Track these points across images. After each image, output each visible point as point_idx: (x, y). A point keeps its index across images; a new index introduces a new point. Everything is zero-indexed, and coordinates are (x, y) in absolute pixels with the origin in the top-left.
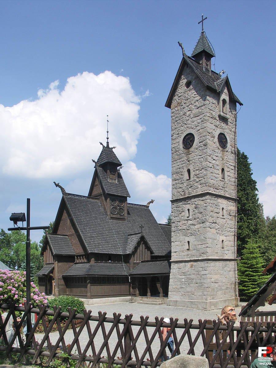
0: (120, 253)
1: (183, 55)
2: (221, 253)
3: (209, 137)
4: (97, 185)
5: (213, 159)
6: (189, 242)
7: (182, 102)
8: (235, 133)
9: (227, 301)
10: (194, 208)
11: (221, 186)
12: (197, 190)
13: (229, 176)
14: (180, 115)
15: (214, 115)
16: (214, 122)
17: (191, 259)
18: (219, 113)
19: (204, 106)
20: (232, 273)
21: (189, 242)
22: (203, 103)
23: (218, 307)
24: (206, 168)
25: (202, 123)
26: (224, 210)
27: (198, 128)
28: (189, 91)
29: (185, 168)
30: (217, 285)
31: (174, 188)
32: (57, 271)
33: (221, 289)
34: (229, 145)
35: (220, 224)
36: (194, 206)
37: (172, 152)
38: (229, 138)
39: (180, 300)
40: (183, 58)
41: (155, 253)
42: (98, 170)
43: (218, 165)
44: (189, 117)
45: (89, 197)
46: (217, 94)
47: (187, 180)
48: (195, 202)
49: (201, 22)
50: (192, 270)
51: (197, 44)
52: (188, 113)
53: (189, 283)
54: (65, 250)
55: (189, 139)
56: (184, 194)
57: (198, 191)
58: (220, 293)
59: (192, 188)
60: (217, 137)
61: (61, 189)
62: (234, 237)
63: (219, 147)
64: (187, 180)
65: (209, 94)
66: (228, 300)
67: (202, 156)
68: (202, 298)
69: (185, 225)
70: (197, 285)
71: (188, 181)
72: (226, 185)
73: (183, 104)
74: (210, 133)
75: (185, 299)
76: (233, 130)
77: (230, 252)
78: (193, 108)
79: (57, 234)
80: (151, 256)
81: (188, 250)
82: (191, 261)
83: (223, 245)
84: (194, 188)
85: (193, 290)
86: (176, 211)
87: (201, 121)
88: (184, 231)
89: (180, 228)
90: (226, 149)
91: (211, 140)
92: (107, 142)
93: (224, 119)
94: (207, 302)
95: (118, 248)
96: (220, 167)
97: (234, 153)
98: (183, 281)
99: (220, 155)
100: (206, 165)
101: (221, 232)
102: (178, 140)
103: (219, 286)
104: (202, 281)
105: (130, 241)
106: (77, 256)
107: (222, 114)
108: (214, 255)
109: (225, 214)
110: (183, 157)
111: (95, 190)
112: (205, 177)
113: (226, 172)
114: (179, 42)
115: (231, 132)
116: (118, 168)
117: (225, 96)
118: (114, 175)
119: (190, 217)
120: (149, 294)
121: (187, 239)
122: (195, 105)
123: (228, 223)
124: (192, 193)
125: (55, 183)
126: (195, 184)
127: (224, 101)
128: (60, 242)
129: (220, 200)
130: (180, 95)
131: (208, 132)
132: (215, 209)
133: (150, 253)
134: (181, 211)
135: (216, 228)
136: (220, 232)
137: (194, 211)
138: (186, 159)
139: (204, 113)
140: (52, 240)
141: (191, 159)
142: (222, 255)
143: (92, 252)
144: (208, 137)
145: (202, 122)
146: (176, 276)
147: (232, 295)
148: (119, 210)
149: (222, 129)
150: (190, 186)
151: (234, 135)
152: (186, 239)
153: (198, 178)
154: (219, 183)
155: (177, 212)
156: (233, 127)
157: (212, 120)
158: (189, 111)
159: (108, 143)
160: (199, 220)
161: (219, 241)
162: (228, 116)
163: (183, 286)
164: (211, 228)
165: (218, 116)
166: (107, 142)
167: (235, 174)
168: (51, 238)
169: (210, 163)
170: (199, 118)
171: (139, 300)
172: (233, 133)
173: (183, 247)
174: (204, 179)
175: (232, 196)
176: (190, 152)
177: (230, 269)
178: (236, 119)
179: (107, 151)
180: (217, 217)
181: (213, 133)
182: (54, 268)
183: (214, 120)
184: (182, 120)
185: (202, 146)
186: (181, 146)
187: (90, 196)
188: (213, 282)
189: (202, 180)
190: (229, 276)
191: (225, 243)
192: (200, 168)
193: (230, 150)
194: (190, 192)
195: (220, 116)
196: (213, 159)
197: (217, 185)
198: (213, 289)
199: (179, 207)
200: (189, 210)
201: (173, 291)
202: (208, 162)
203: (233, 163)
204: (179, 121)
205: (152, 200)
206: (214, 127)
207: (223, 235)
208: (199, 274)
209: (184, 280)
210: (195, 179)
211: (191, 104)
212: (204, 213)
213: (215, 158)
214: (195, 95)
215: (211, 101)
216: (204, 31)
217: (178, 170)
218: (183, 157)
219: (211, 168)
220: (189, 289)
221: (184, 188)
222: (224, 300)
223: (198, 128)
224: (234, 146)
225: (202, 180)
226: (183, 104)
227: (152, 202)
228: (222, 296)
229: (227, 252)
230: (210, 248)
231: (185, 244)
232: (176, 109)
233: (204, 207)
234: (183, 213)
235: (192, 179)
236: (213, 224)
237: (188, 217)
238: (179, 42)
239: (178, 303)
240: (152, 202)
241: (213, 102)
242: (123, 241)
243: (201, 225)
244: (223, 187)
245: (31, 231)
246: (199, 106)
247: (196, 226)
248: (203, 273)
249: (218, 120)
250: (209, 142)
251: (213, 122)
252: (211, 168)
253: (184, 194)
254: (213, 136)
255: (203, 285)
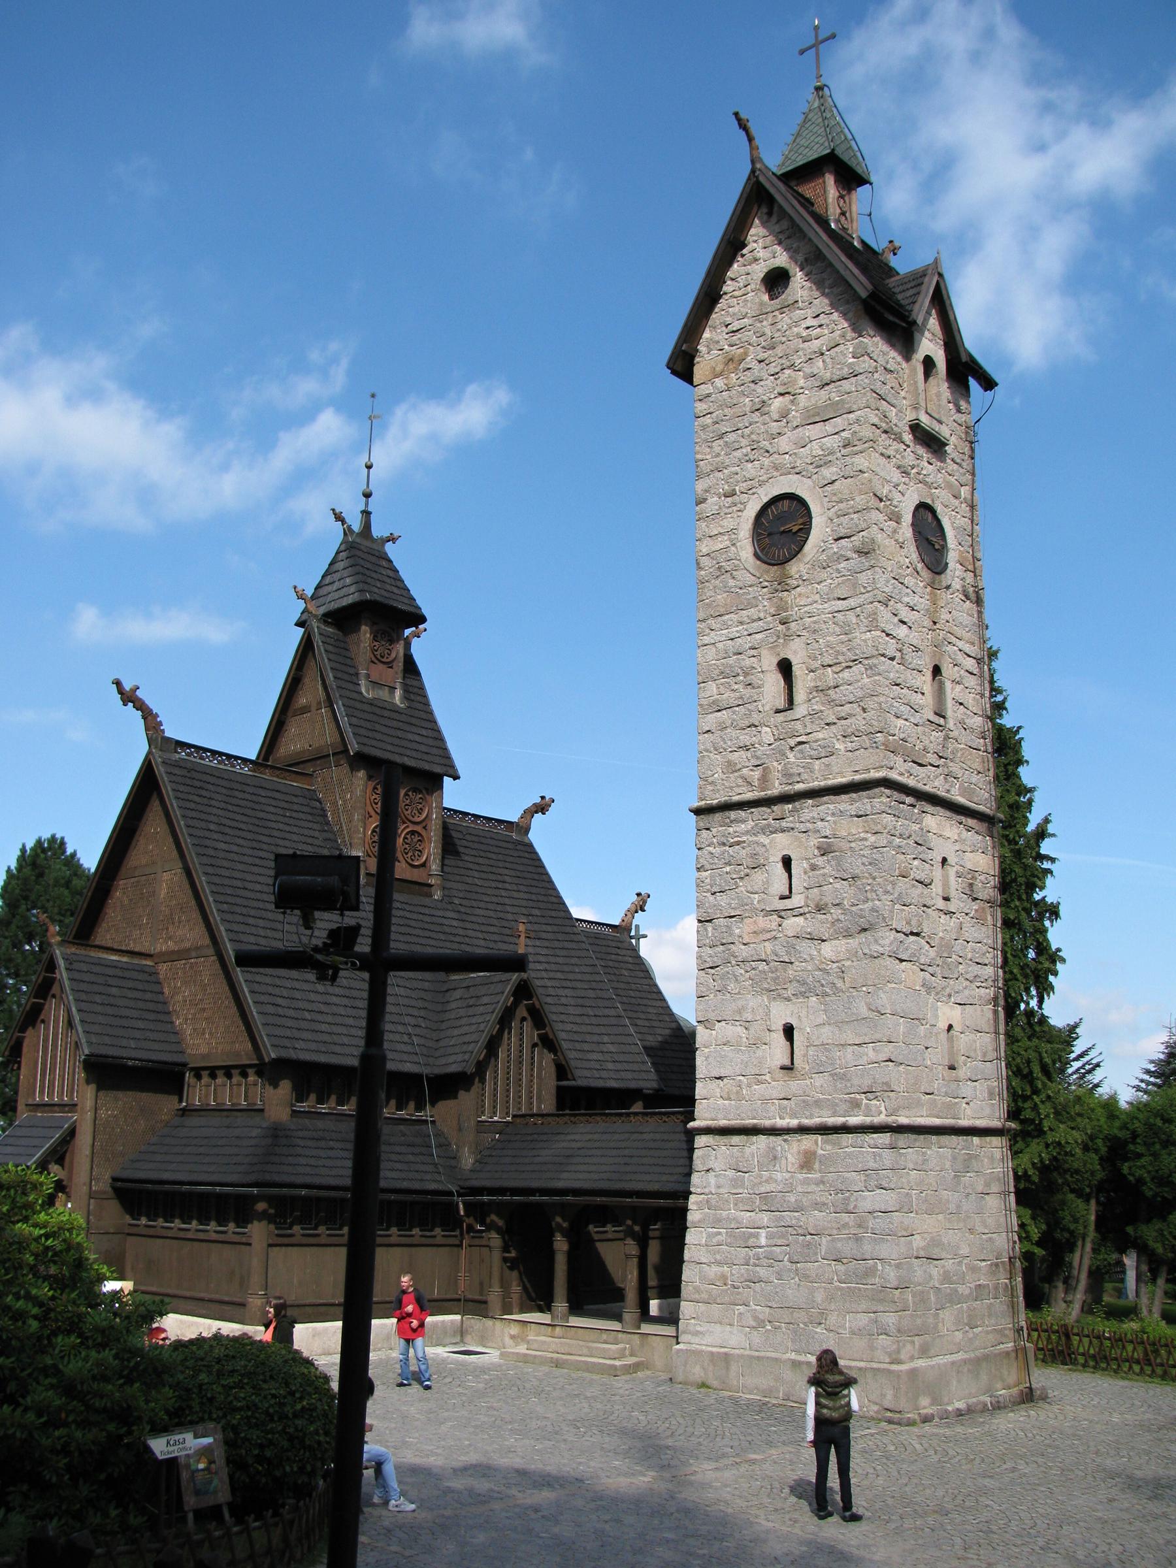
0: (414, 1069)
1: (753, 162)
2: (946, 1094)
3: (881, 517)
4: (305, 710)
5: (896, 620)
6: (789, 1031)
7: (746, 354)
8: (972, 507)
9: (984, 1364)
10: (816, 852)
11: (932, 747)
12: (828, 765)
13: (961, 704)
14: (738, 410)
15: (894, 421)
16: (897, 451)
17: (807, 1122)
18: (910, 416)
19: (853, 380)
20: (993, 1203)
21: (789, 1031)
22: (850, 365)
23: (946, 1400)
24: (875, 661)
25: (844, 451)
26: (952, 872)
27: (828, 473)
28: (781, 309)
29: (764, 652)
30: (935, 1271)
31: (709, 746)
32: (88, 1152)
33: (954, 1298)
34: (952, 557)
35: (937, 941)
36: (814, 841)
37: (703, 573)
38: (952, 523)
39: (748, 1352)
40: (753, 171)
41: (577, 1073)
42: (317, 640)
43: (917, 650)
44: (783, 423)
45: (261, 765)
46: (902, 334)
47: (778, 711)
48: (819, 823)
49: (810, 48)
50: (806, 1182)
51: (798, 128)
52: (778, 403)
53: (795, 1259)
54: (137, 1034)
55: (782, 518)
56: (764, 780)
57: (835, 769)
58: (947, 1315)
59: (801, 752)
60: (908, 518)
61: (144, 718)
62: (996, 1012)
63: (920, 566)
64: (778, 711)
65: (872, 333)
66: (986, 1358)
67: (852, 602)
68: (872, 1348)
69: (768, 936)
70: (840, 1267)
71: (780, 717)
72: (951, 745)
73: (750, 361)
74: (881, 500)
75: (776, 1351)
76: (964, 492)
77: (981, 1088)
78: (801, 382)
79: (97, 943)
80: (560, 1089)
81: (788, 1068)
82: (803, 1130)
83: (952, 1052)
84: (813, 753)
85: (819, 1297)
86: (720, 864)
87: (841, 444)
88: (762, 966)
89: (743, 952)
90: (946, 579)
91: (889, 531)
92: (363, 512)
93: (931, 442)
94: (898, 1374)
95: (406, 1038)
96: (928, 660)
97: (973, 596)
98: (763, 1241)
99: (923, 603)
100: (870, 643)
101: (943, 983)
102: (728, 523)
103: (946, 1277)
104: (867, 1249)
105: (659, 1031)
106: (197, 1073)
107: (925, 420)
108: (919, 1104)
109: (953, 894)
110: (753, 601)
111: (293, 728)
112: (870, 704)
113: (948, 685)
114: (736, 114)
115: (956, 502)
116: (407, 632)
117: (930, 345)
118: (389, 664)
119: (797, 900)
120: (561, 1306)
121: (781, 1014)
122: (808, 370)
123: (967, 936)
124: (805, 776)
125: (118, 683)
126: (820, 735)
127: (929, 363)
128: (114, 991)
129: (935, 821)
130: (736, 325)
131: (875, 495)
132: (916, 863)
133: (554, 1076)
134: (749, 862)
135: (922, 961)
136: (937, 982)
137: (814, 868)
138: (772, 611)
139: (855, 407)
140: (76, 976)
141: (793, 612)
142: (950, 1106)
143: (284, 1054)
144: (875, 516)
145: (844, 446)
146: (724, 1213)
147: (1001, 1332)
148: (405, 838)
149: (925, 483)
150: (792, 742)
151: (968, 515)
152: (773, 1011)
153: (832, 702)
154: (924, 733)
155: (728, 869)
156: (963, 480)
157: (887, 443)
158: (781, 394)
159: (366, 514)
160: (842, 917)
161: (935, 1030)
162: (944, 431)
163: (762, 1272)
164: (902, 961)
165: (911, 427)
166: (363, 512)
167: (982, 696)
168: (75, 966)
169: (888, 635)
170: (829, 427)
171: (507, 1340)
172: (963, 505)
173: (759, 1053)
174: (864, 710)
175: (975, 799)
176: (789, 581)
177: (987, 1185)
178: (972, 450)
179: (362, 552)
180: (924, 906)
181: (895, 503)
182: (72, 1133)
183: (896, 445)
184: (747, 431)
185: (850, 554)
186: (746, 551)
187: (266, 759)
188: (922, 1254)
189: (851, 715)
190: (984, 1223)
191: (963, 1041)
192: (841, 658)
193: (957, 585)
194: (795, 770)
195: (915, 428)
196: (896, 620)
197: (919, 747)
198: (922, 1299)
199: (738, 843)
200: (787, 862)
201: (705, 1296)
202: (879, 633)
203: (973, 644)
204: (731, 437)
205: (543, 798)
206: (896, 476)
207: (950, 996)
208: (851, 1207)
209: (769, 1237)
210: (815, 707)
211: (789, 368)
212: (870, 881)
213: (905, 614)
214: (808, 328)
215: (881, 361)
216: (823, 81)
217: (731, 661)
218: (753, 601)
219: (892, 659)
220: (793, 1291)
221: (761, 750)
222: (970, 1360)
223: (828, 473)
224: (971, 567)
225: (851, 715)
226: (754, 364)
227: (542, 807)
228: (959, 1335)
229: (967, 1089)
230: (901, 1068)
231: (768, 1037)
232: (719, 383)
233: (866, 852)
234: (758, 877)
235: (800, 710)
236: (912, 938)
237: (782, 898)
238: (736, 114)
239: (734, 1367)
240: (542, 807)
241: (888, 366)
242: (420, 1004)
243: (853, 943)
244: (941, 757)
245: (399, 984)
246: (828, 376)
247: (828, 950)
248: (871, 1200)
249: (908, 446)
250: (880, 537)
251: (891, 452)
252: (892, 659)
253: (764, 780)
254: (893, 513)
255: (871, 1272)
